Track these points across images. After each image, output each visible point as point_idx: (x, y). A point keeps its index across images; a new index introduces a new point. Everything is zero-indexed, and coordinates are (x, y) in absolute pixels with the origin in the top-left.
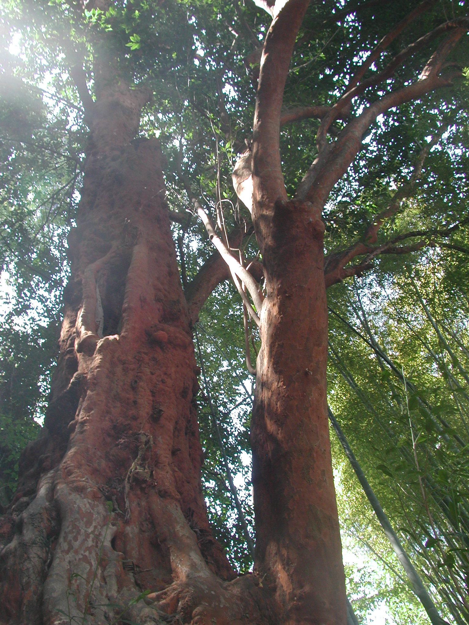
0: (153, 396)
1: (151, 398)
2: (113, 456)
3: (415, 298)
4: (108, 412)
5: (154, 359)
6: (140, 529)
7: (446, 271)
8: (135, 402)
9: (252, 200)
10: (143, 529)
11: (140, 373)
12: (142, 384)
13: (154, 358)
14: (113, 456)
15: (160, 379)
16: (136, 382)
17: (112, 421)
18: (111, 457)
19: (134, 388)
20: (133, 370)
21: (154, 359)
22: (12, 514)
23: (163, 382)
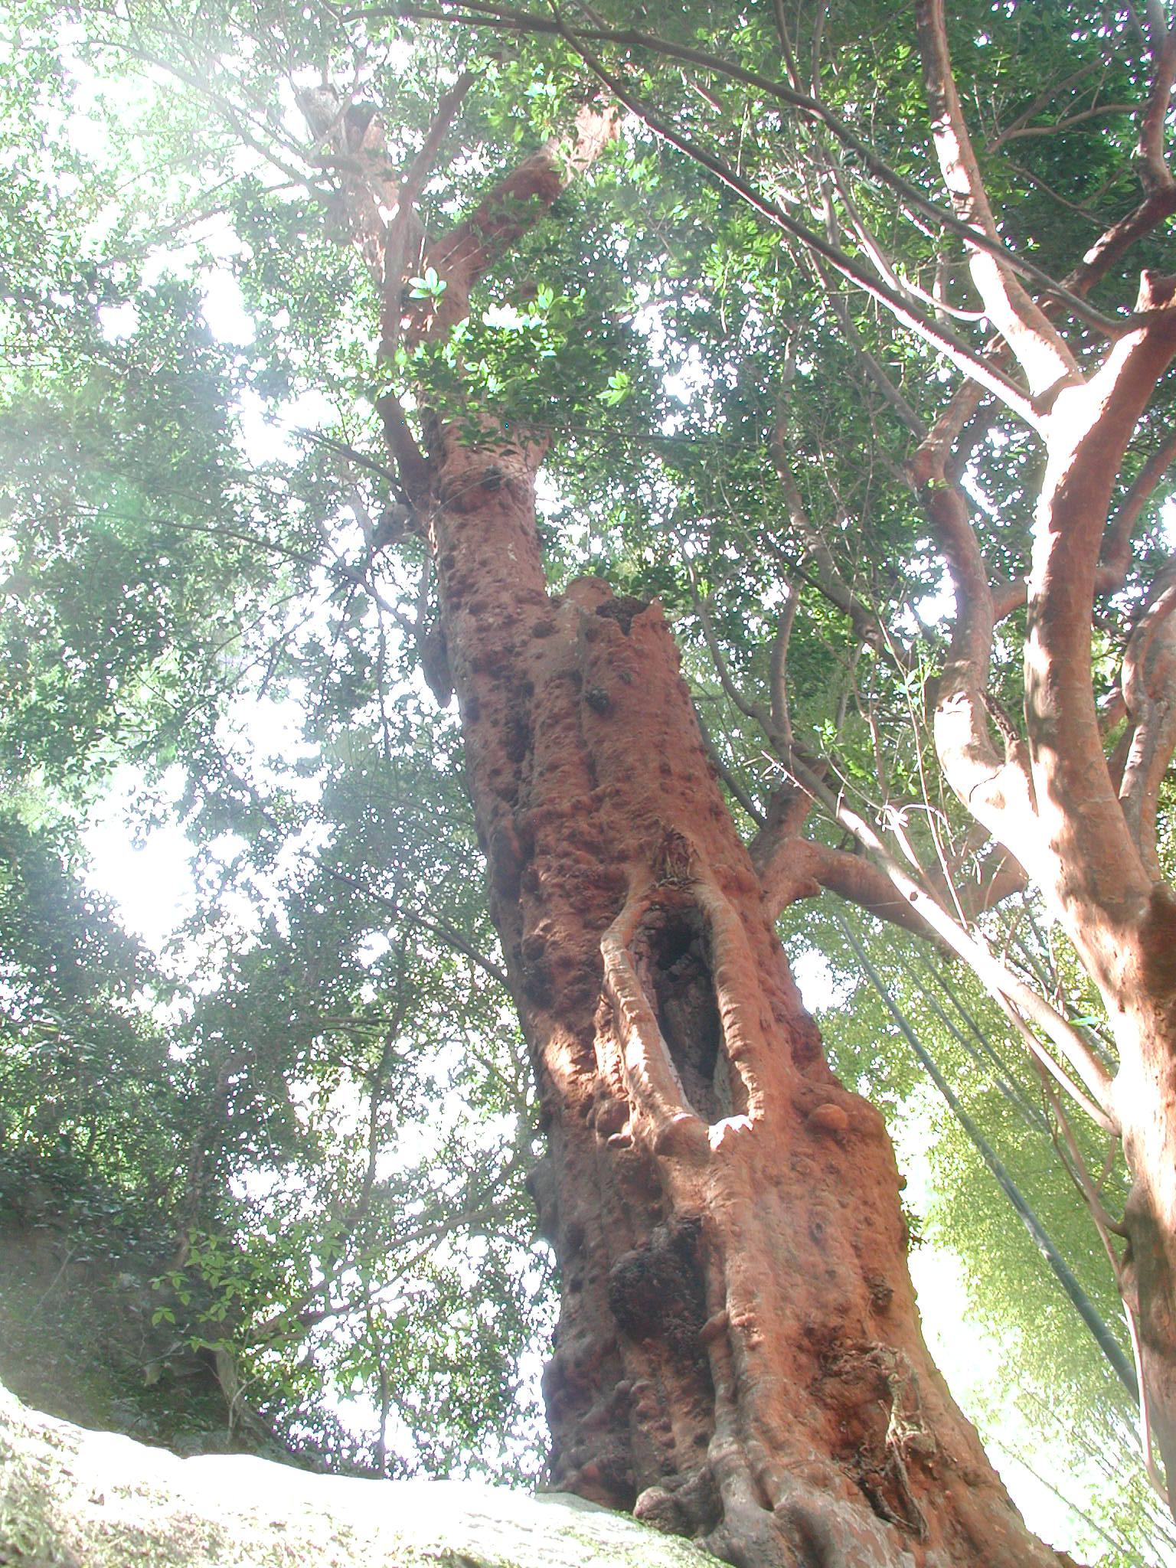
0: (859, 1256)
1: (856, 1261)
2: (832, 1397)
3: (634, 351)
4: (785, 1298)
5: (832, 1170)
6: (952, 1555)
7: (212, 58)
8: (831, 1274)
9: (1012, 1493)
10: (957, 1554)
11: (821, 1204)
12: (830, 1230)
13: (832, 1167)
14: (832, 1397)
15: (862, 1218)
16: (819, 1226)
17: (797, 1317)
18: (829, 1400)
19: (818, 1240)
20: (802, 1198)
21: (832, 1170)
22: (867, 316)
23: (868, 1222)
